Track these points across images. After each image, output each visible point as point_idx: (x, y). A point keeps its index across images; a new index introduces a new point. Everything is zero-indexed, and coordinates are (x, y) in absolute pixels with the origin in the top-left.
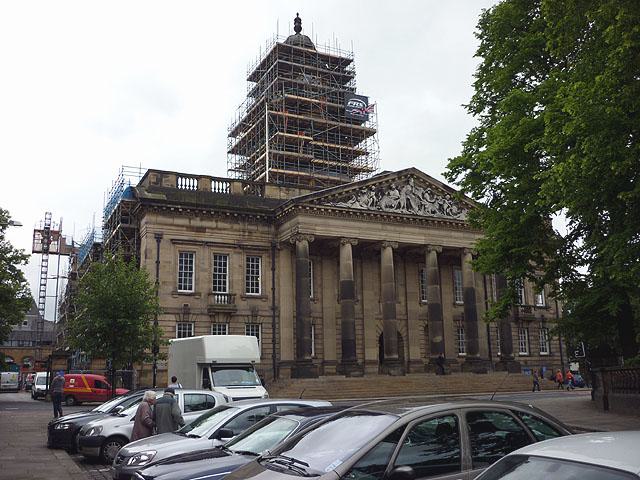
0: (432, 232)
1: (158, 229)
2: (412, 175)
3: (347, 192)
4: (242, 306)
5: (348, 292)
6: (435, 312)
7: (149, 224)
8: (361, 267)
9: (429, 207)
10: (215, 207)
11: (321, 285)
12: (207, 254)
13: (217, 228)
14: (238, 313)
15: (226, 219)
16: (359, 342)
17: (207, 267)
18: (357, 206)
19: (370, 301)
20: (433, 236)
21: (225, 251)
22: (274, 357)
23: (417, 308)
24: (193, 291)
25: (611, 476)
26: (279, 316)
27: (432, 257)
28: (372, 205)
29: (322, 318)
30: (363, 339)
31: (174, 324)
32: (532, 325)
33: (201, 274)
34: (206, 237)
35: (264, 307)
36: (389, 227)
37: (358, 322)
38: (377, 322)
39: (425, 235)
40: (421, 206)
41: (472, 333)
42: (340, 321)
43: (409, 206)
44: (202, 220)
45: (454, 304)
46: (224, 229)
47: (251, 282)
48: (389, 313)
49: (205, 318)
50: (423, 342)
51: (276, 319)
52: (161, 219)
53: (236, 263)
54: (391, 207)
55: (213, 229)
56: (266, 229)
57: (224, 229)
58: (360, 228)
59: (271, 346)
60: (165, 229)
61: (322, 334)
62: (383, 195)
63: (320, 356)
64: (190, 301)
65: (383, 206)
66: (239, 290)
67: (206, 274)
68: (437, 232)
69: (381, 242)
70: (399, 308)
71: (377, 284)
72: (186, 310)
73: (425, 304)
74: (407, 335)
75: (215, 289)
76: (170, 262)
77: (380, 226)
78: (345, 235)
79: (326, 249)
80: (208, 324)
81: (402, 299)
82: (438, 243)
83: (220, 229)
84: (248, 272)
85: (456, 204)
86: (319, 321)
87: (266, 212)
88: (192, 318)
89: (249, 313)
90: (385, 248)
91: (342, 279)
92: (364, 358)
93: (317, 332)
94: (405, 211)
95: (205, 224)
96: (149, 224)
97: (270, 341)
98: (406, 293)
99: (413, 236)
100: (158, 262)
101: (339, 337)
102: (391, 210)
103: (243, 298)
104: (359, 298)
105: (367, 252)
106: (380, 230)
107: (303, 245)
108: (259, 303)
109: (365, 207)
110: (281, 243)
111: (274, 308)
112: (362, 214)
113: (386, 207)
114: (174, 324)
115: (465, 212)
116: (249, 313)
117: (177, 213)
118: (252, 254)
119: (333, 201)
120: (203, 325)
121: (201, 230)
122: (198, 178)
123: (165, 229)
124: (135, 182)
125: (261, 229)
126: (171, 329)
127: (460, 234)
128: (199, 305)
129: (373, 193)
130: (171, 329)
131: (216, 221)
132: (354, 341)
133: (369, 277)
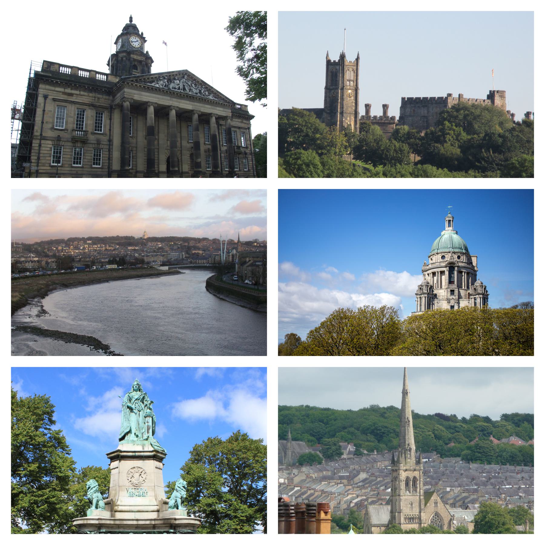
0: (196, 104)
1: (45, 92)
2: (186, 74)
3: (152, 78)
4: (92, 138)
5: (151, 132)
6: (197, 145)
7: (43, 89)
8: (158, 121)
9: (195, 91)
10: (79, 83)
11: (137, 130)
12: (73, 108)
13: (80, 95)
14: (89, 142)
15: (85, 90)
16: (156, 161)
17: (72, 115)
18: (157, 86)
19: (163, 140)
20: (197, 106)
21: (85, 107)
22: (109, 168)
23: (187, 144)
24: (102, 132)
25: (261, 271)
26: (112, 145)
27: (196, 117)
28: (165, 86)
29: (136, 147)
30: (158, 160)
31: (51, 146)
32: (241, 156)
33: (69, 119)
34: (73, 99)
35: (104, 139)
36: (174, 99)
37: (156, 150)
38: (166, 151)
39: (192, 105)
40: (190, 90)
41: (215, 158)
42: (146, 149)
43: (184, 89)
44: (71, 89)
45: (205, 144)
46: (84, 95)
47: (98, 126)
48: (173, 145)
49: (70, 144)
50: (189, 162)
51: (111, 146)
52: (48, 87)
53: (90, 115)
54: (175, 88)
55: (77, 95)
56: (107, 97)
57: (84, 95)
58: (158, 98)
59: (107, 161)
60: (49, 93)
61: (136, 156)
62: (171, 82)
63: (134, 168)
64: (62, 134)
65: (171, 87)
66: (90, 129)
67: (72, 119)
68: (198, 104)
69: (169, 106)
70: (178, 144)
71: (166, 131)
72: (59, 138)
73: (190, 143)
74: (181, 159)
75: (77, 127)
76: (51, 111)
77: (169, 98)
78: (150, 101)
79: (139, 109)
80: (71, 147)
81: (179, 139)
82: (199, 110)
83: (82, 95)
84: (96, 120)
85: (207, 91)
86: (135, 149)
87: (108, 88)
88: (61, 143)
89: (96, 142)
90: (149, 106)
91: (148, 125)
92: (159, 170)
93: (134, 155)
94: (182, 91)
95: (73, 92)
96: (43, 89)
97: (107, 159)
98: (181, 136)
99: (186, 105)
100: (44, 111)
101: (146, 158)
102: (176, 90)
103: (93, 134)
104: (157, 137)
105: (162, 112)
106: (168, 100)
107: (127, 104)
108: (102, 137)
109: (161, 87)
110: (115, 105)
111: (110, 141)
112: (160, 90)
113: (173, 88)
114: (51, 146)
115: (212, 95)
116: (96, 142)
117: (56, 84)
118: (99, 110)
119: (144, 82)
120: (68, 147)
121: (71, 95)
122: (71, 67)
123: (49, 93)
124: (39, 69)
125: (104, 97)
126: (49, 149)
127: (222, 109)
128: (66, 136)
129: (166, 80)
130: (49, 149)
131: (80, 91)
132: (154, 160)
133: (163, 127)
